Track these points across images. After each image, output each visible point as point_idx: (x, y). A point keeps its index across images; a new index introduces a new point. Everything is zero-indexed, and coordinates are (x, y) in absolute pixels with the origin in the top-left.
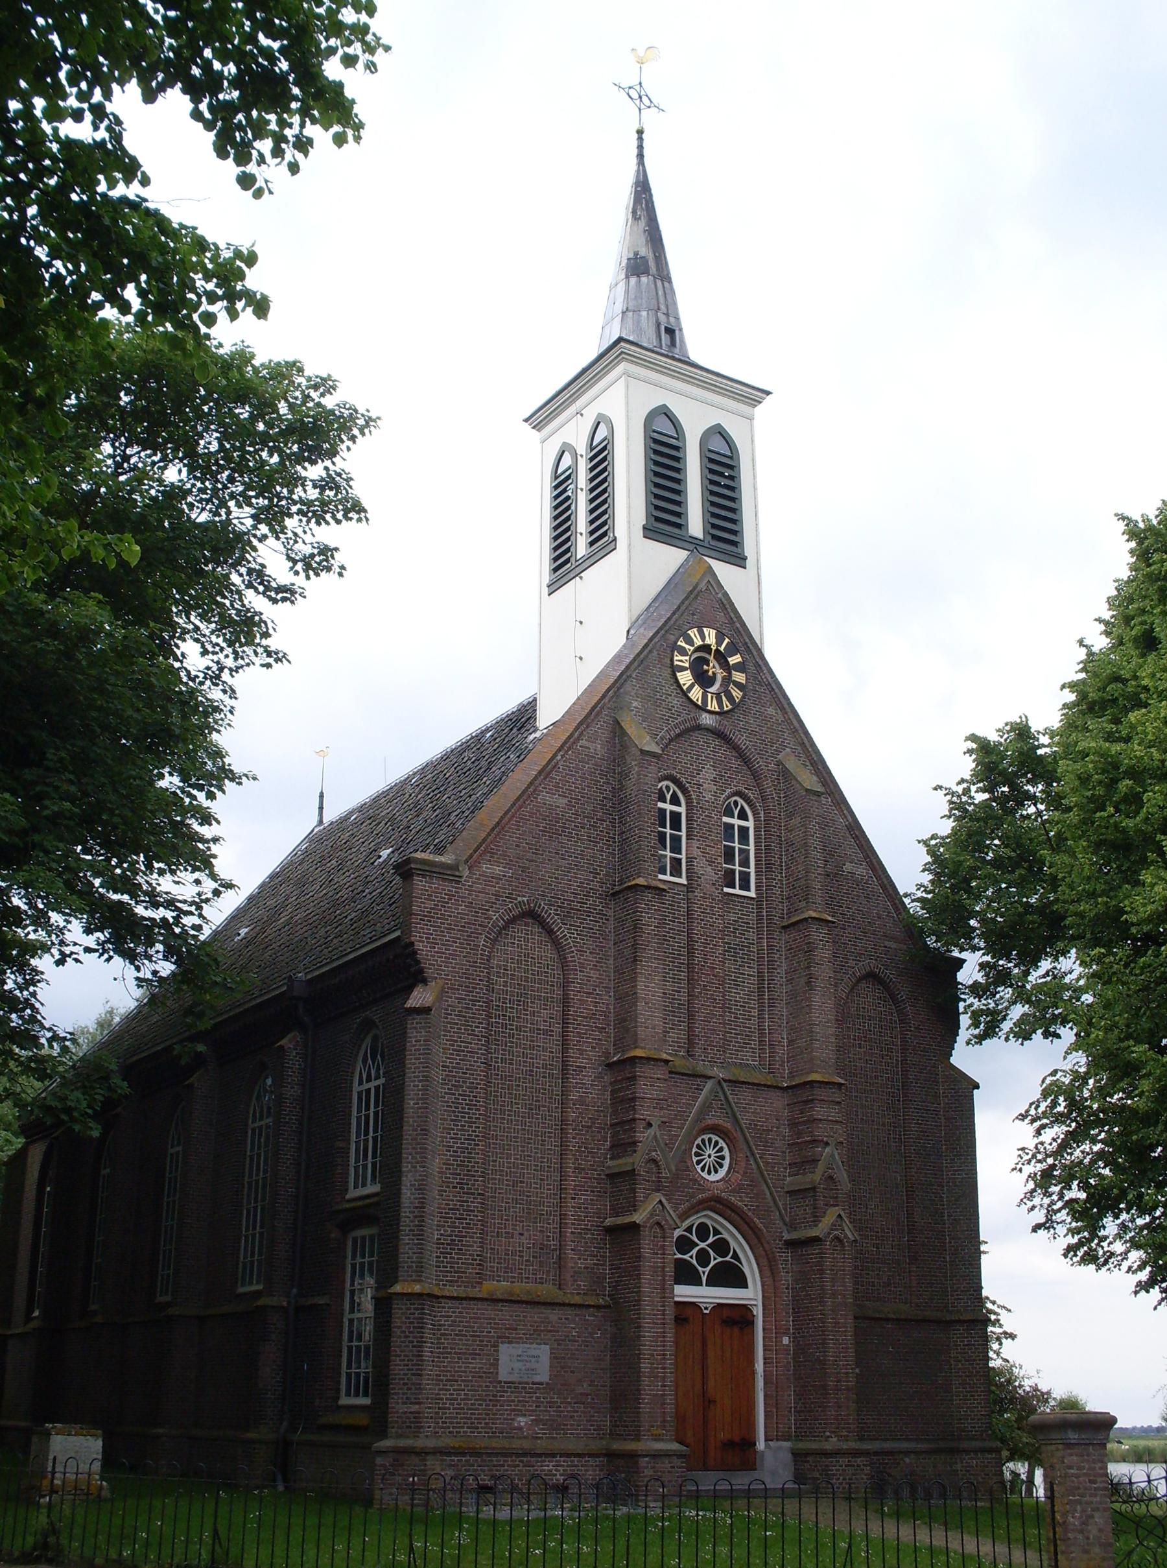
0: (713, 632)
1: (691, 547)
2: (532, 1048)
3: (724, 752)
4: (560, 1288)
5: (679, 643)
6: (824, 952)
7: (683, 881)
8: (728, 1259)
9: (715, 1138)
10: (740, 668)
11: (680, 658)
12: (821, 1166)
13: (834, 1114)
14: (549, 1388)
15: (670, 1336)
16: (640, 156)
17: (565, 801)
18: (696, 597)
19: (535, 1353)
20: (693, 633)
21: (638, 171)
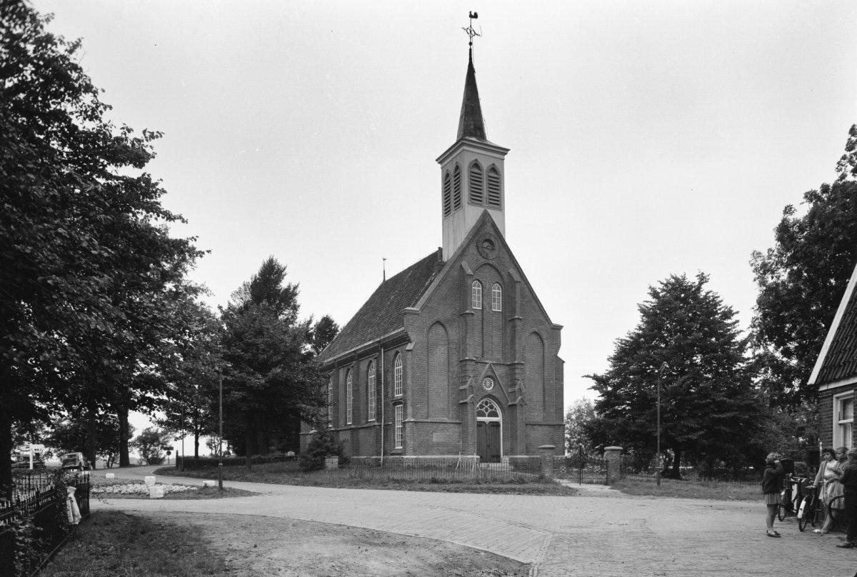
12: (468, 383)
15: (476, 430)
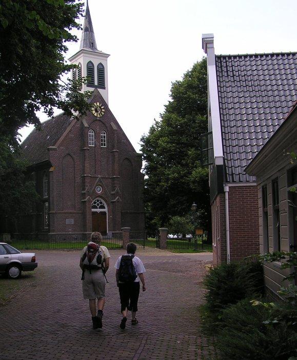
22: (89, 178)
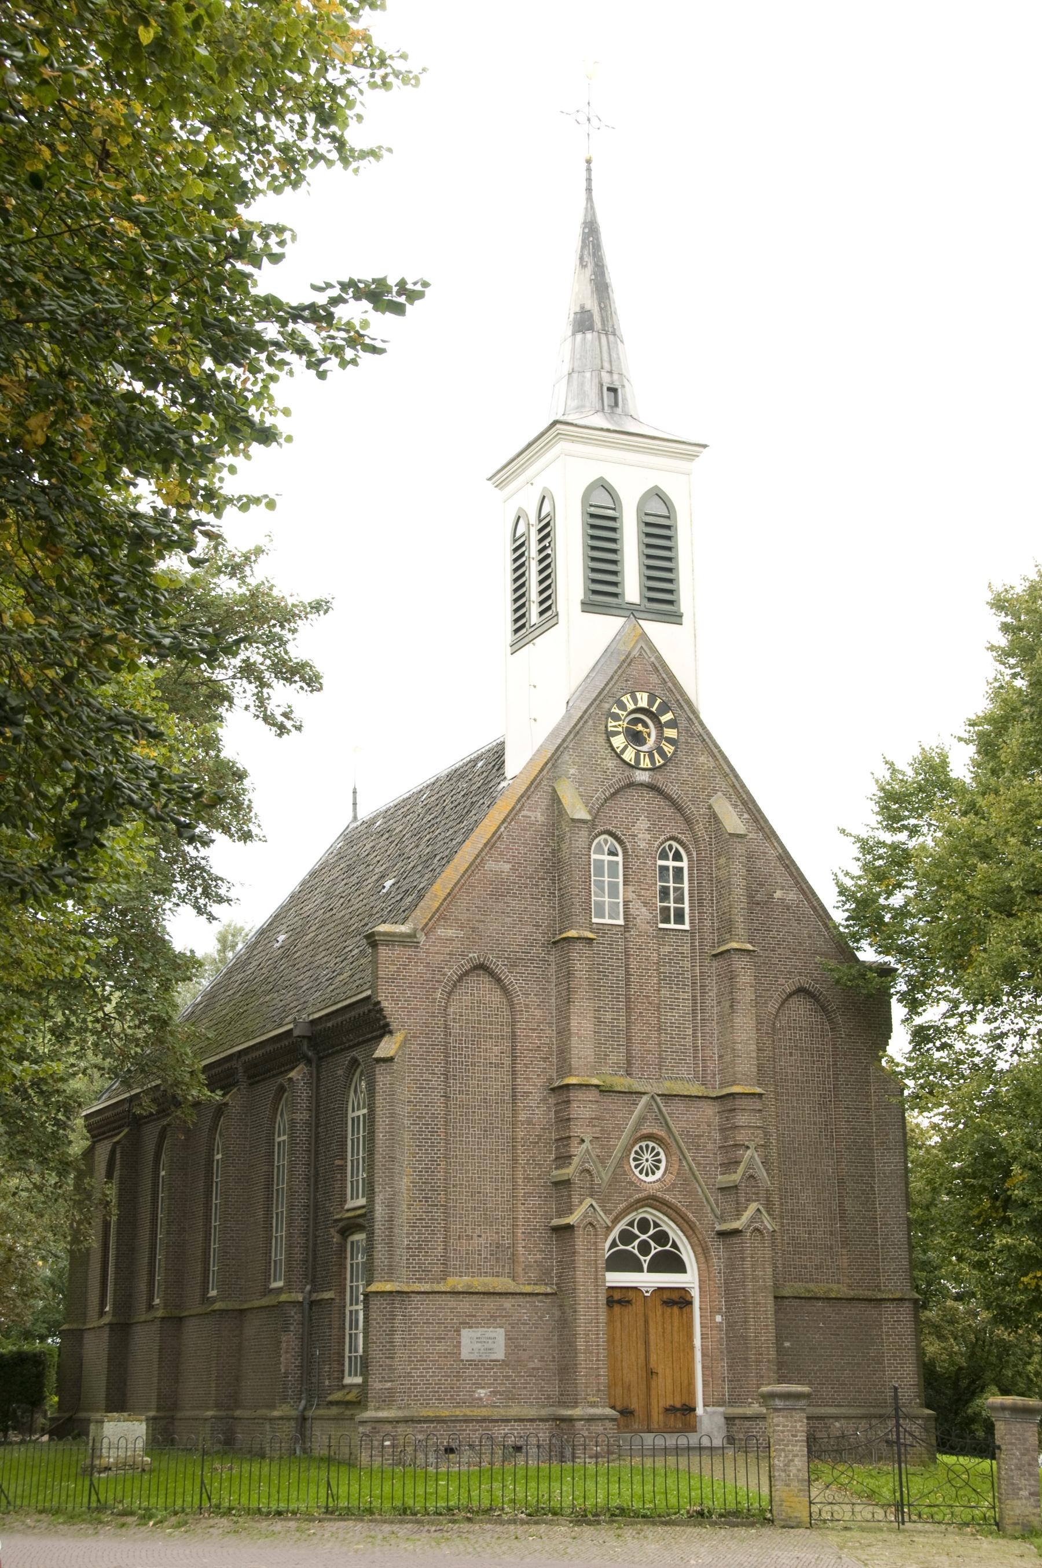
0: (645, 696)
1: (627, 613)
2: (485, 1079)
3: (659, 802)
4: (514, 1280)
5: (613, 710)
6: (745, 978)
7: (621, 922)
8: (667, 1248)
9: (651, 1144)
10: (672, 724)
11: (614, 724)
13: (756, 1120)
14: (505, 1363)
16: (589, 190)
17: (509, 866)
18: (629, 665)
19: (493, 1335)
20: (626, 699)
21: (586, 209)
22: (593, 1095)
